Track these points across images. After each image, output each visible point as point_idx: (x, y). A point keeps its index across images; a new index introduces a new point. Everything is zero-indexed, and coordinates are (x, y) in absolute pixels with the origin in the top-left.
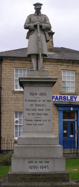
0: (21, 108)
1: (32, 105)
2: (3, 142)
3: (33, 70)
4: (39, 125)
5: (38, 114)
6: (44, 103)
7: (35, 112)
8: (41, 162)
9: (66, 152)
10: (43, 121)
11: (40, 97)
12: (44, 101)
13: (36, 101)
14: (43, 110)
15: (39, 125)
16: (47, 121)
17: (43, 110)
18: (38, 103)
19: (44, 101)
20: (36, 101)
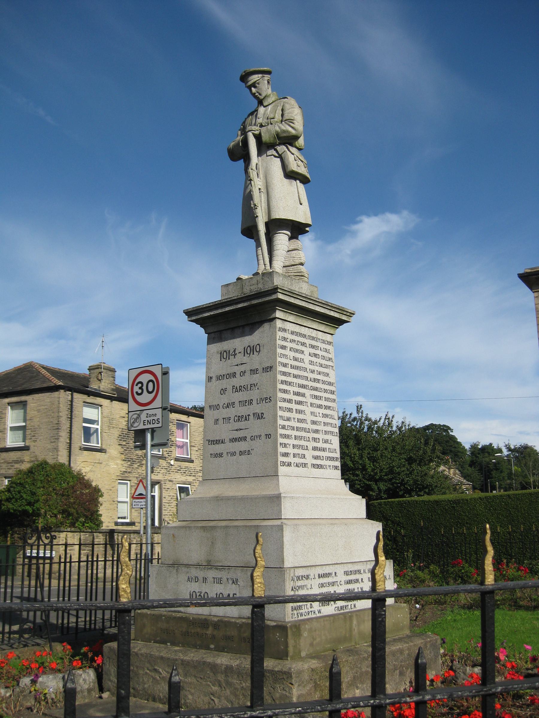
0: (108, 613)
1: (223, 391)
2: (144, 546)
3: (177, 420)
4: (241, 453)
5: (240, 418)
6: (255, 378)
7: (231, 412)
8: (219, 581)
9: (41, 555)
10: (253, 438)
11: (245, 359)
12: (254, 371)
13: (234, 375)
14: (251, 402)
15: (241, 453)
16: (263, 437)
17: (251, 402)
18: (237, 381)
19: (254, 371)
20: (234, 375)
